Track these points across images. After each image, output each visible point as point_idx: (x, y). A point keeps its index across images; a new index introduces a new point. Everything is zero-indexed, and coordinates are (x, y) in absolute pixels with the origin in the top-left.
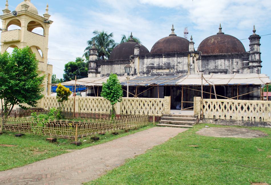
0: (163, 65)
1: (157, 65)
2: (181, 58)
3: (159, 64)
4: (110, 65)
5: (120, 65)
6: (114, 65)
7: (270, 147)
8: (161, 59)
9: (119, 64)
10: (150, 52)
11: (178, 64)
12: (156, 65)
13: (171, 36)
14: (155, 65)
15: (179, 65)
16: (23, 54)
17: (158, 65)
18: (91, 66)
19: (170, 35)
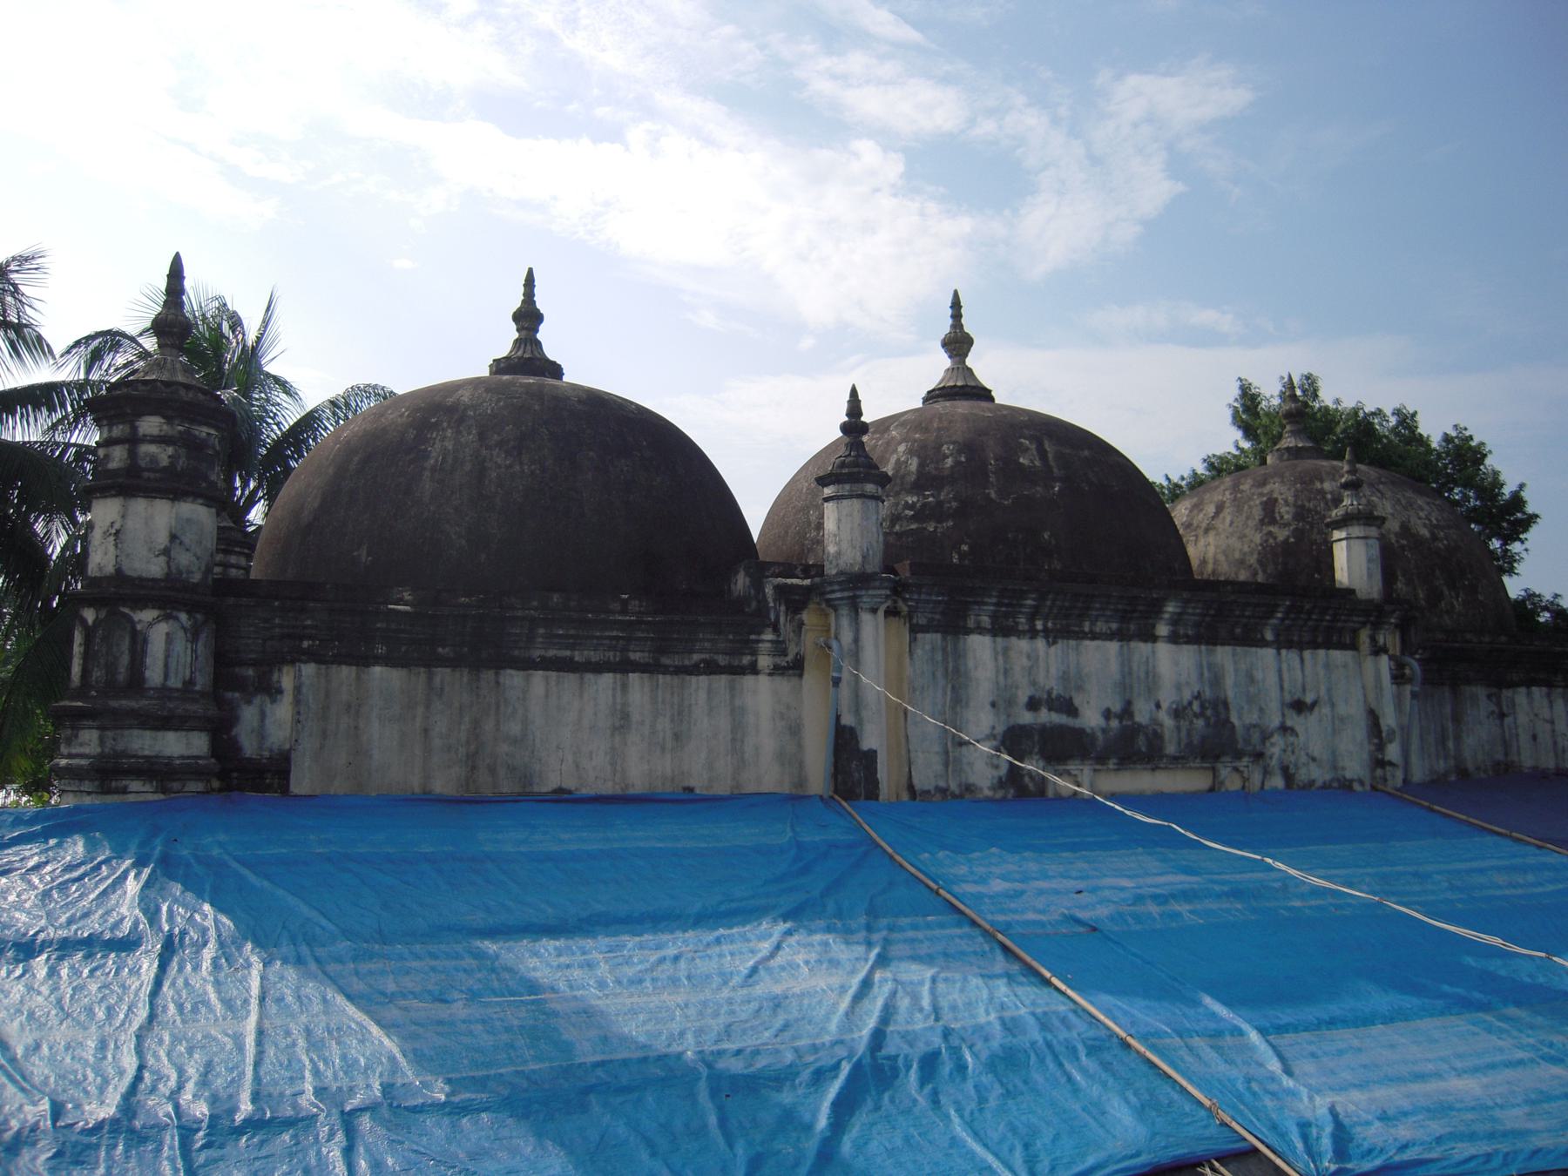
0: (1168, 722)
1: (1107, 714)
2: (1307, 654)
3: (1127, 711)
4: (454, 663)
5: (607, 679)
6: (513, 679)
7: (3, 1014)
8: (1141, 648)
9: (598, 668)
10: (755, 528)
11: (1293, 720)
12: (1101, 722)
13: (942, 406)
14: (1091, 718)
15: (1298, 729)
16: (499, 400)
17: (1120, 717)
18: (154, 674)
19: (932, 396)
